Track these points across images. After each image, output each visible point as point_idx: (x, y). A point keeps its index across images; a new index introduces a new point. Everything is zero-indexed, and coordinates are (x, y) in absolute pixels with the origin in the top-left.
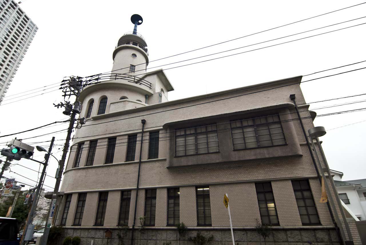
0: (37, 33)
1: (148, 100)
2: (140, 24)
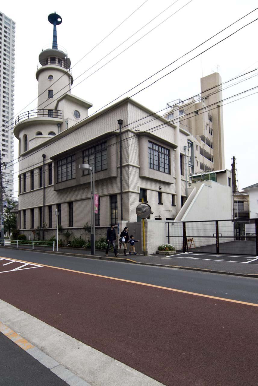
0: (16, 30)
1: (61, 128)
2: (59, 23)
